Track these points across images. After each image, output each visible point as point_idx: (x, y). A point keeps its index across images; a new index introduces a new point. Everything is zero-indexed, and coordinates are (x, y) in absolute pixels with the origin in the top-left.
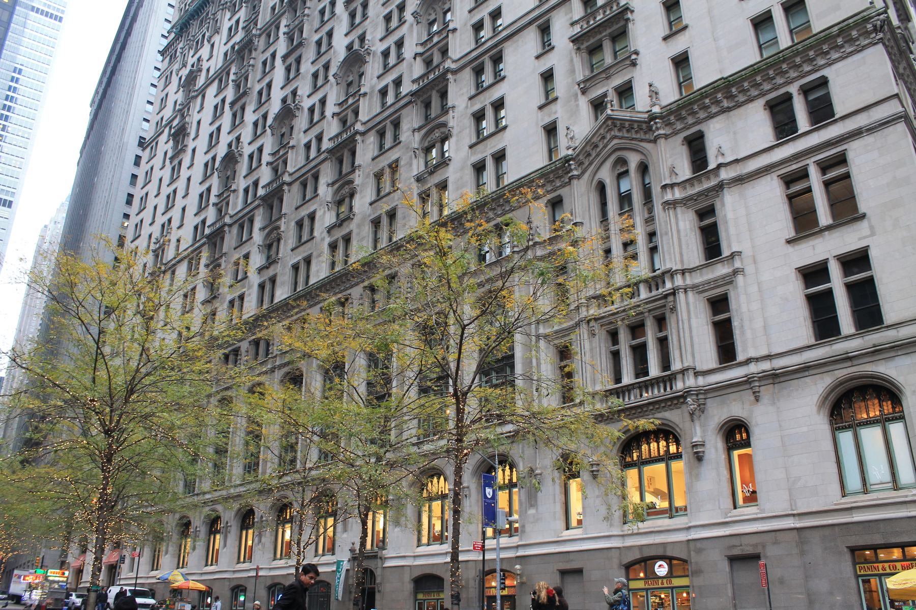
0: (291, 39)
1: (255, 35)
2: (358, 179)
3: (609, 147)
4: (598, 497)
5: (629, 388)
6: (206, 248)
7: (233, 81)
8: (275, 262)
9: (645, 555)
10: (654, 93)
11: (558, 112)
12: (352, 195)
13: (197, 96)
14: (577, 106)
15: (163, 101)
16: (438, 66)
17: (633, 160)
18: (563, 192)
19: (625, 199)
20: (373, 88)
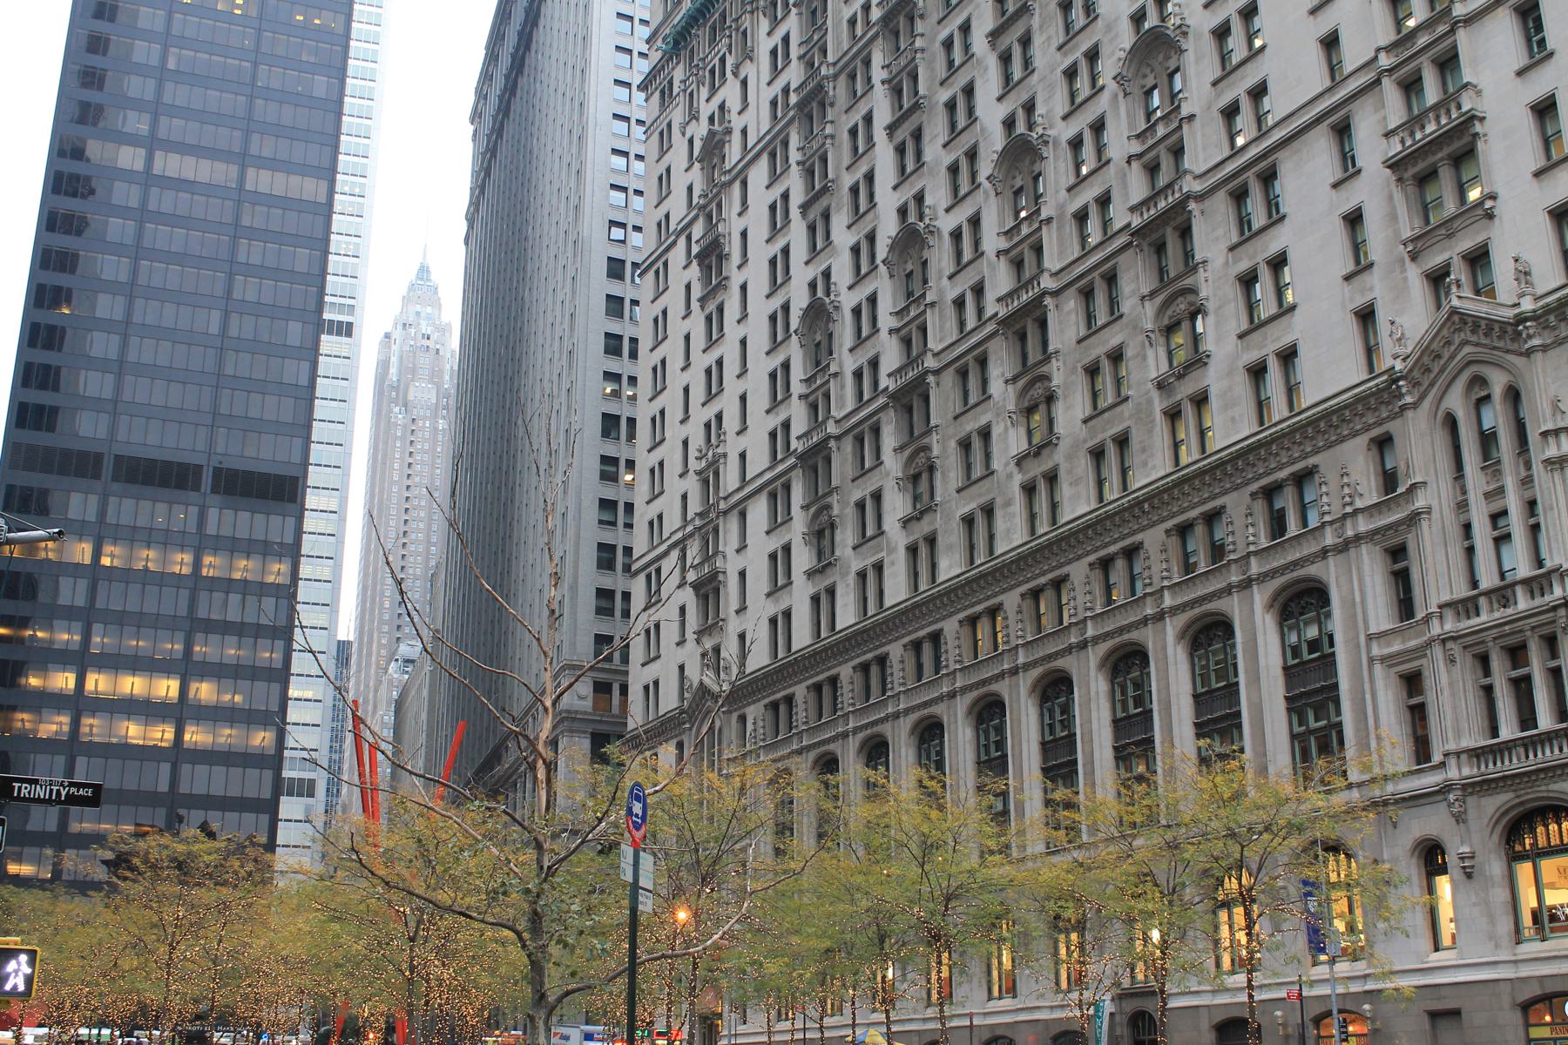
0: (897, 92)
1: (827, 77)
2: (1058, 374)
3: (1459, 357)
4: (1474, 905)
5: (1509, 746)
6: (798, 473)
7: (798, 163)
8: (929, 510)
9: (1548, 991)
10: (1524, 275)
11: (1376, 287)
12: (1050, 399)
13: (731, 182)
14: (1405, 279)
15: (665, 179)
16: (1170, 185)
17: (1498, 382)
18: (1392, 427)
19: (1487, 440)
20: (1061, 208)
